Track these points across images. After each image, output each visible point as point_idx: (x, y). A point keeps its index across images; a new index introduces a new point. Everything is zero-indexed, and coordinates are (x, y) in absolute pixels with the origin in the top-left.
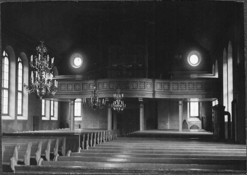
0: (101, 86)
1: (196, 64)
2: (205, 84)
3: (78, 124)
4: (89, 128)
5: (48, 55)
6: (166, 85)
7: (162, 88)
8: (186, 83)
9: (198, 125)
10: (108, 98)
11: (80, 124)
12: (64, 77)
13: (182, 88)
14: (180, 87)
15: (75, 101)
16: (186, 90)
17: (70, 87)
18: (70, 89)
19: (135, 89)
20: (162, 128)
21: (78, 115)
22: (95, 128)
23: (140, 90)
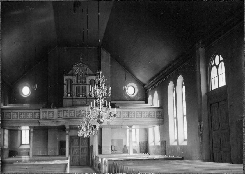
0: (30, 116)
1: (29, 94)
4: (37, 155)
5: (109, 85)
7: (148, 116)
8: (25, 112)
10: (68, 126)
11: (29, 152)
12: (12, 106)
13: (131, 116)
14: (130, 116)
16: (148, 117)
19: (9, 119)
20: (106, 153)
21: (133, 140)
22: (44, 155)
23: (59, 118)
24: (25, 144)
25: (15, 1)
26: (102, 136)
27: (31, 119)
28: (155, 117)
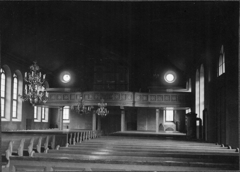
10: (93, 106)
11: (68, 125)
12: (54, 89)
13: (159, 99)
16: (163, 101)
21: (66, 119)
24: (65, 120)
25: (168, 1)
26: (173, 115)
27: (61, 100)
28: (141, 100)
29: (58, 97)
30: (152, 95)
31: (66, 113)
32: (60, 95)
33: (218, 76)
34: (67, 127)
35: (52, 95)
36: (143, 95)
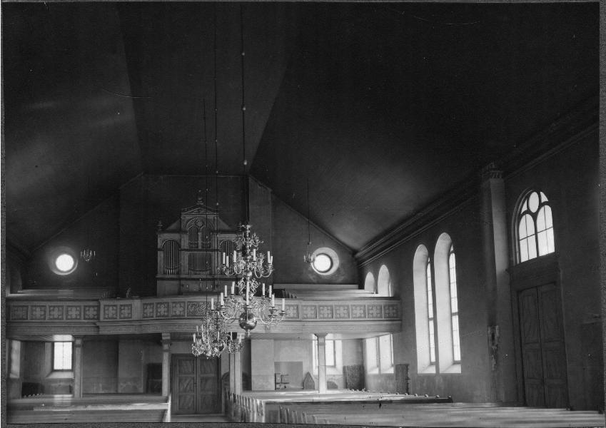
2: (386, 308)
3: (68, 384)
5: (269, 253)
6: (292, 308)
9: (336, 383)
10: (169, 334)
12: (31, 292)
15: (327, 337)
17: (74, 313)
18: (74, 316)
24: (62, 371)
26: (71, 358)
29: (70, 313)
30: (307, 306)
31: (63, 353)
32: (76, 307)
33: (518, 262)
34: (68, 389)
35: (54, 307)
36: (145, 304)
